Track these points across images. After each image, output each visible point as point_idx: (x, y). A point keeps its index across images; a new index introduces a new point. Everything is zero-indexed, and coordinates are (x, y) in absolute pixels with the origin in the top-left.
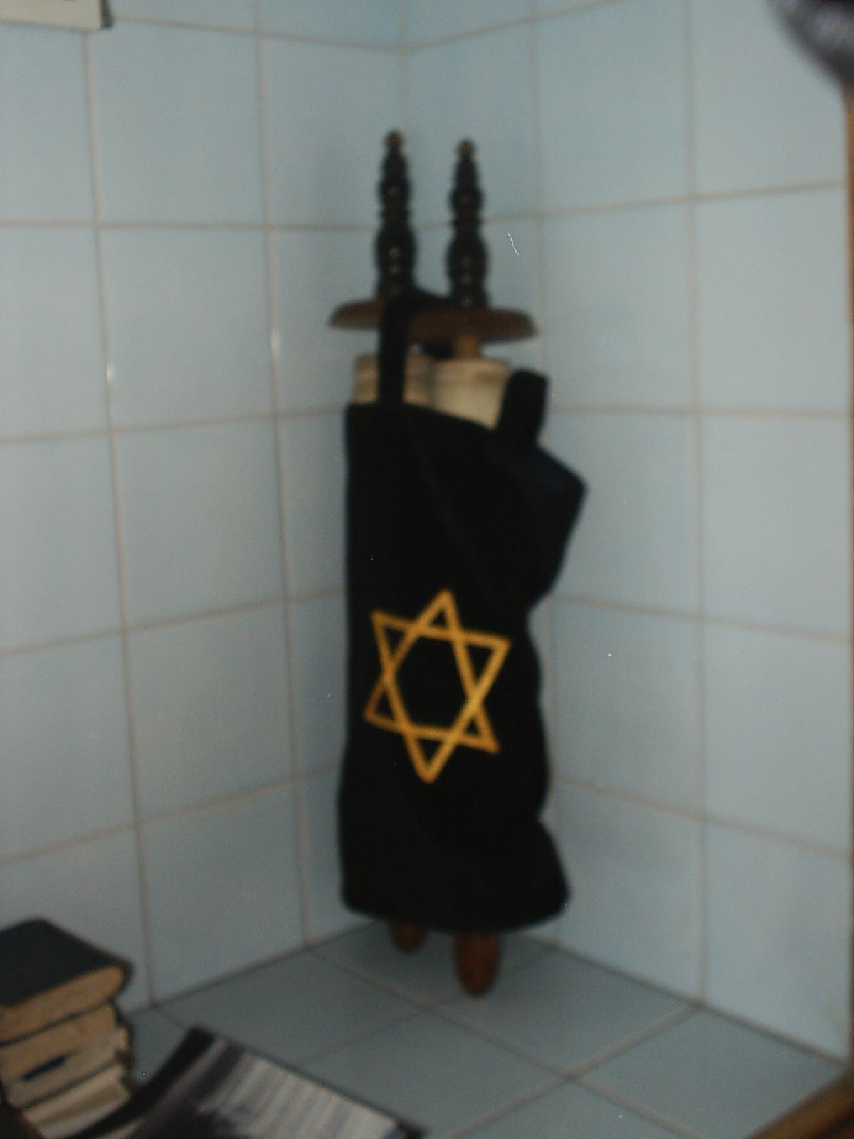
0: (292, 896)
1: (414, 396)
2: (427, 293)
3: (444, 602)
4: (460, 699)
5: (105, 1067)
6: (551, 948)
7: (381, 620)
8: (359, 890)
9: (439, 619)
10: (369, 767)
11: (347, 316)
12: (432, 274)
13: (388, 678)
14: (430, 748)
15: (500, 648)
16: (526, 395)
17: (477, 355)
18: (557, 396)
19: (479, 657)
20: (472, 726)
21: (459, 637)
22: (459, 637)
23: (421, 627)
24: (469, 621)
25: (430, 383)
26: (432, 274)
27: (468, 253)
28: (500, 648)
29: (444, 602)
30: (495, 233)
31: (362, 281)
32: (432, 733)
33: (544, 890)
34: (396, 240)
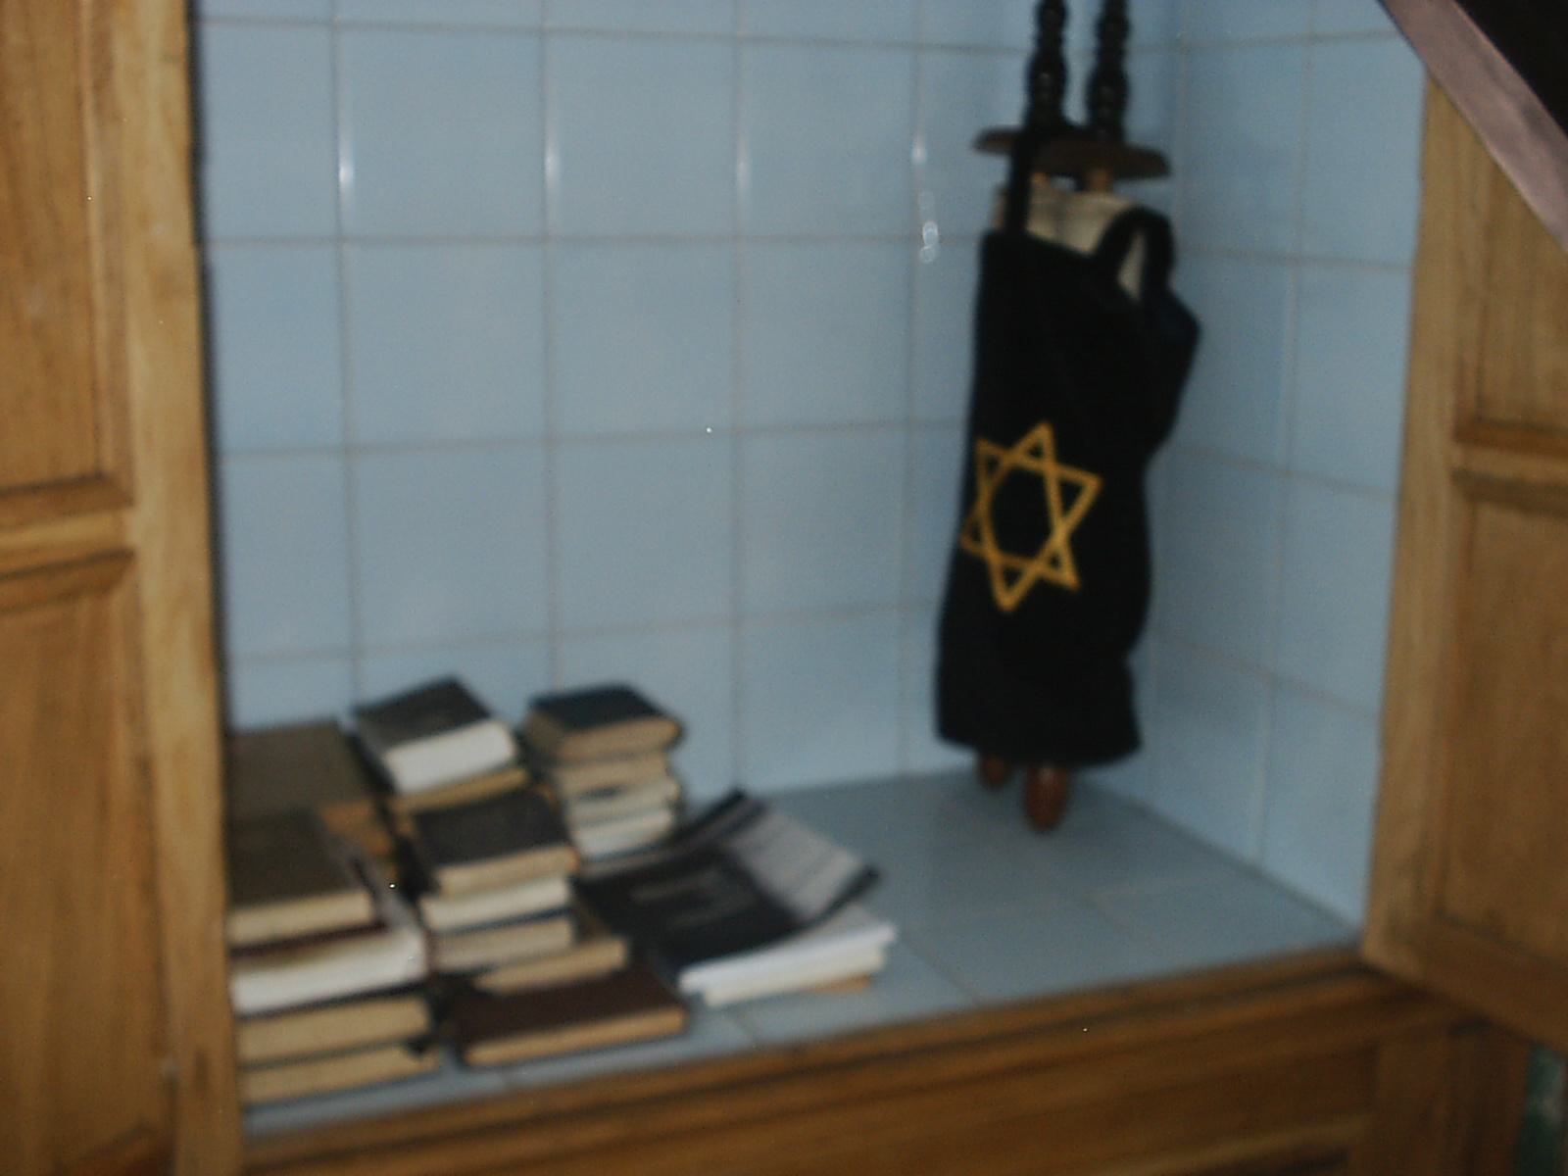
0: (887, 730)
1: (1040, 228)
2: (1069, 130)
3: (1042, 434)
4: (1044, 531)
5: (486, 1068)
6: (1140, 813)
7: (986, 448)
8: (955, 719)
9: (1036, 451)
10: (966, 580)
11: (991, 141)
12: (1075, 109)
13: (983, 505)
14: (1011, 577)
15: (1090, 485)
16: (1150, 234)
17: (1108, 189)
18: (1180, 232)
19: (1070, 493)
20: (1056, 561)
21: (1051, 471)
22: (1051, 471)
23: (1017, 457)
24: (1066, 454)
25: (1058, 215)
26: (1075, 109)
27: (1110, 83)
28: (1090, 485)
29: (1042, 434)
30: (1142, 68)
31: (1010, 109)
32: (1015, 562)
33: (1118, 737)
34: (1046, 69)
